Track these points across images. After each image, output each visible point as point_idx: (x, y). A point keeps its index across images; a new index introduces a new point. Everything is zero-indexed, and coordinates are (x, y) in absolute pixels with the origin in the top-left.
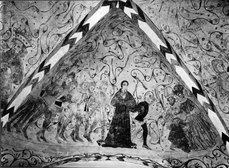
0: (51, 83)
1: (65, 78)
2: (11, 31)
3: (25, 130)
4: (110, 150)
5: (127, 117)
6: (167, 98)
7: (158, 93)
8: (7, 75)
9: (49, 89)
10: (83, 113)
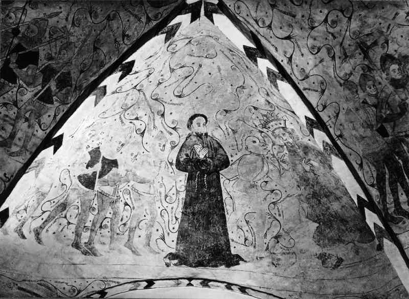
0: (374, 109)
1: (384, 75)
2: (263, 132)
8: (319, 169)
9: (384, 116)
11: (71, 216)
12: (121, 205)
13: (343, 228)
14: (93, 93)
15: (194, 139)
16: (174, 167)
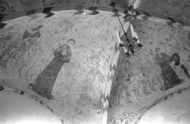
2: (88, 59)
3: (119, 103)
4: (167, 92)
5: (169, 67)
6: (187, 44)
7: (180, 44)
10: (143, 78)
11: (7, 44)
12: (27, 53)
13: (89, 102)
14: (78, 10)
15: (66, 47)
16: (53, 51)
